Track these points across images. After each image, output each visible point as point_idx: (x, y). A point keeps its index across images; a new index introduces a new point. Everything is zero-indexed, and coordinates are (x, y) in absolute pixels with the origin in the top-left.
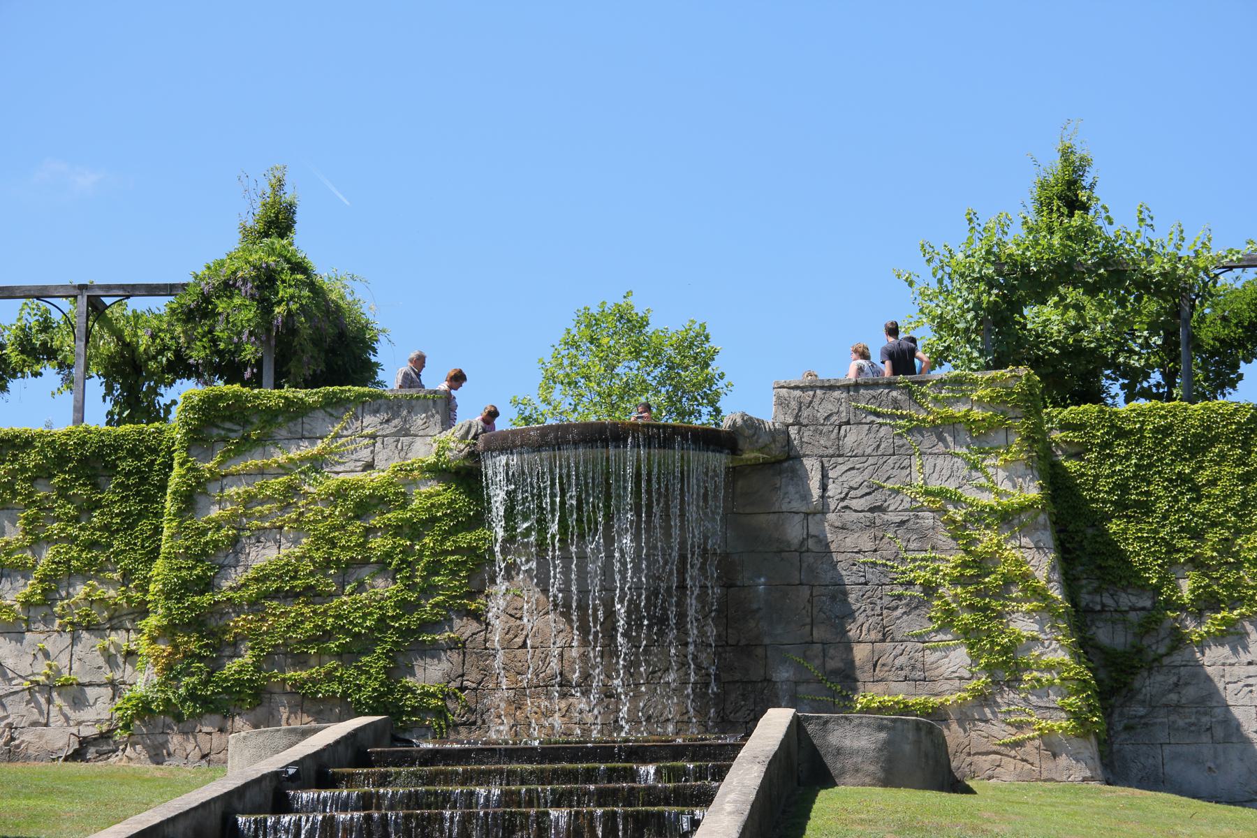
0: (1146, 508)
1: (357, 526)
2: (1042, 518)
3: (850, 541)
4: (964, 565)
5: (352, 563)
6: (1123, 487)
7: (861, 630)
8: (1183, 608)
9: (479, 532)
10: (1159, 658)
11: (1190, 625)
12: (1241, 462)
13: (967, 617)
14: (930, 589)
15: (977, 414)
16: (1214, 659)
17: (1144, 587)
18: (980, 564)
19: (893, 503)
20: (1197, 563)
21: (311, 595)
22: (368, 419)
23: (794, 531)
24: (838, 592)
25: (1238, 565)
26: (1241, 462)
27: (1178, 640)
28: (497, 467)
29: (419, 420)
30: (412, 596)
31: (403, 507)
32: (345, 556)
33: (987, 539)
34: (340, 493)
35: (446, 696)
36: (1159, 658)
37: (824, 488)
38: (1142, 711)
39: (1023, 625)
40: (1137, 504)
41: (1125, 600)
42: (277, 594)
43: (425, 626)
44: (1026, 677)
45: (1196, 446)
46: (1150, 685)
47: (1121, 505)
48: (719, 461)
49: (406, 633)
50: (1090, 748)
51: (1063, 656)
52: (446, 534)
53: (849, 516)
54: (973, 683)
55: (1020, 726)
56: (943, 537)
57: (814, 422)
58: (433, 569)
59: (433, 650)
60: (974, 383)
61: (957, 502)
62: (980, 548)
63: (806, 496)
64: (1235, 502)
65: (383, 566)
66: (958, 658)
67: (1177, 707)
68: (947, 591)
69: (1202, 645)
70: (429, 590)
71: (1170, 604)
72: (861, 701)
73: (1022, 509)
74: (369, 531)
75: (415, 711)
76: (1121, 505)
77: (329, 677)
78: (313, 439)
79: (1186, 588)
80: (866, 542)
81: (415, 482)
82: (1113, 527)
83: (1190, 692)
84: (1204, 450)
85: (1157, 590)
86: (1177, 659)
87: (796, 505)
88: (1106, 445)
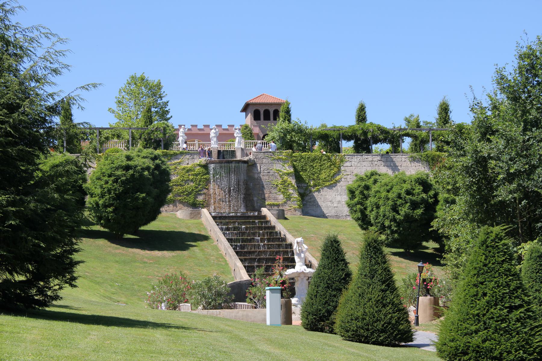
0: (306, 170)
1: (187, 174)
2: (294, 174)
3: (265, 177)
4: (282, 182)
5: (187, 180)
6: (303, 167)
7: (266, 191)
8: (311, 186)
9: (207, 176)
10: (308, 194)
11: (312, 189)
12: (320, 163)
13: (283, 190)
14: (277, 185)
15: (284, 157)
16: (316, 194)
17: (306, 183)
18: (285, 182)
19: (271, 171)
20: (314, 179)
21: (181, 185)
22: (187, 156)
23: (256, 176)
24: (263, 187)
25: (319, 180)
26: (320, 163)
27: (311, 191)
28: (212, 166)
29: (195, 156)
30: (197, 186)
31: (194, 171)
32: (186, 179)
33: (285, 177)
34: (184, 169)
35: (203, 202)
36: (308, 194)
37: (260, 169)
38: (305, 202)
39: (291, 191)
40: (305, 170)
41: (303, 185)
42: (175, 185)
43: (200, 191)
44: (292, 199)
45: (313, 160)
46: (307, 198)
47: (302, 170)
48: (246, 165)
49: (196, 192)
50: (301, 210)
51: (297, 196)
52: (202, 176)
53: (264, 173)
54: (284, 200)
55: (290, 207)
56: (279, 177)
57: (258, 158)
58: (200, 181)
59: (201, 194)
60: (283, 152)
61: (281, 172)
62: (284, 179)
63: (258, 170)
64: (319, 170)
65: (192, 181)
66: (281, 196)
67: (310, 202)
68: (280, 186)
69: (314, 192)
70: (199, 185)
71: (310, 186)
72: (267, 203)
73: (291, 173)
74: (189, 175)
75: (199, 204)
76: (302, 170)
77: (185, 198)
78: (178, 159)
79: (312, 183)
80: (267, 178)
81: (196, 167)
82: (301, 173)
83: (312, 200)
84: (315, 161)
85: (308, 183)
86: (310, 194)
87: (256, 172)
88: (300, 160)
